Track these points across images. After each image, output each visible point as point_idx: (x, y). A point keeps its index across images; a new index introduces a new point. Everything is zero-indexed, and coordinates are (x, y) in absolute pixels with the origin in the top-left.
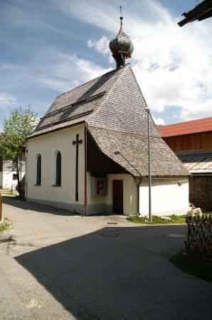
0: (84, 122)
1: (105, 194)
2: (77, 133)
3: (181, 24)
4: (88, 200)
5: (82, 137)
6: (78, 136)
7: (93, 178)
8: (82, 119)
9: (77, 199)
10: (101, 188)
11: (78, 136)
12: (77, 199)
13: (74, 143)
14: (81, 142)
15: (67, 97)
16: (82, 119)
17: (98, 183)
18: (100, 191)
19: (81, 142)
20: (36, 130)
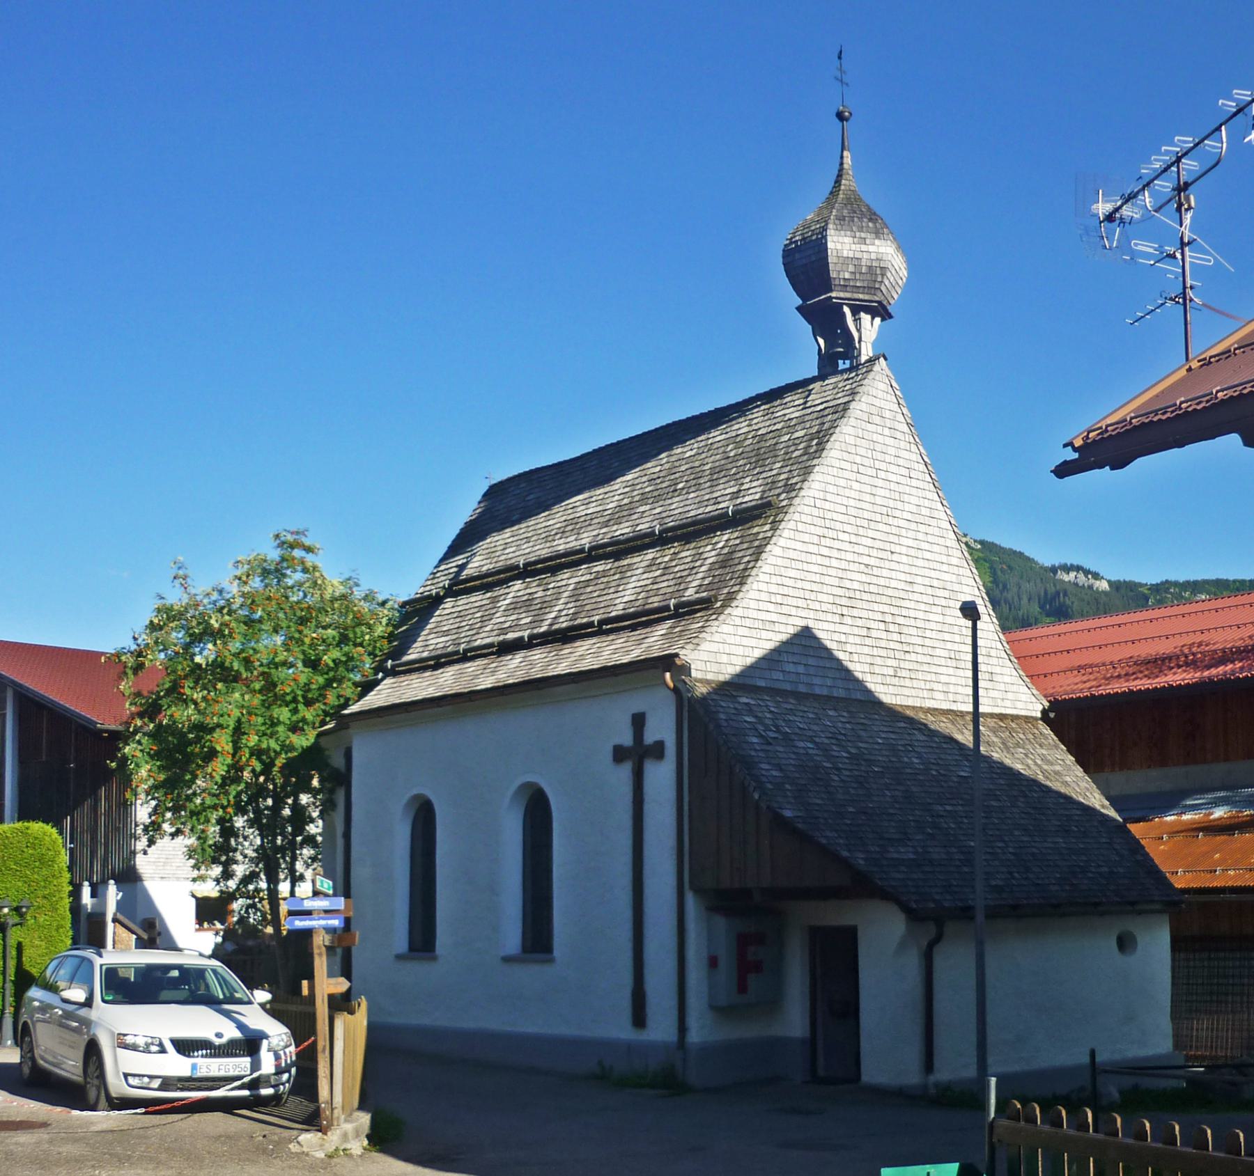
0: (667, 662)
1: (772, 1004)
2: (637, 707)
3: (1063, 470)
4: (693, 1022)
5: (662, 728)
6: (639, 721)
7: (721, 922)
8: (653, 642)
9: (639, 1019)
10: (758, 967)
11: (639, 721)
12: (639, 1019)
13: (620, 754)
14: (657, 751)
15: (625, 536)
16: (653, 642)
17: (743, 942)
18: (752, 979)
19: (657, 751)
20: (25, 1023)
